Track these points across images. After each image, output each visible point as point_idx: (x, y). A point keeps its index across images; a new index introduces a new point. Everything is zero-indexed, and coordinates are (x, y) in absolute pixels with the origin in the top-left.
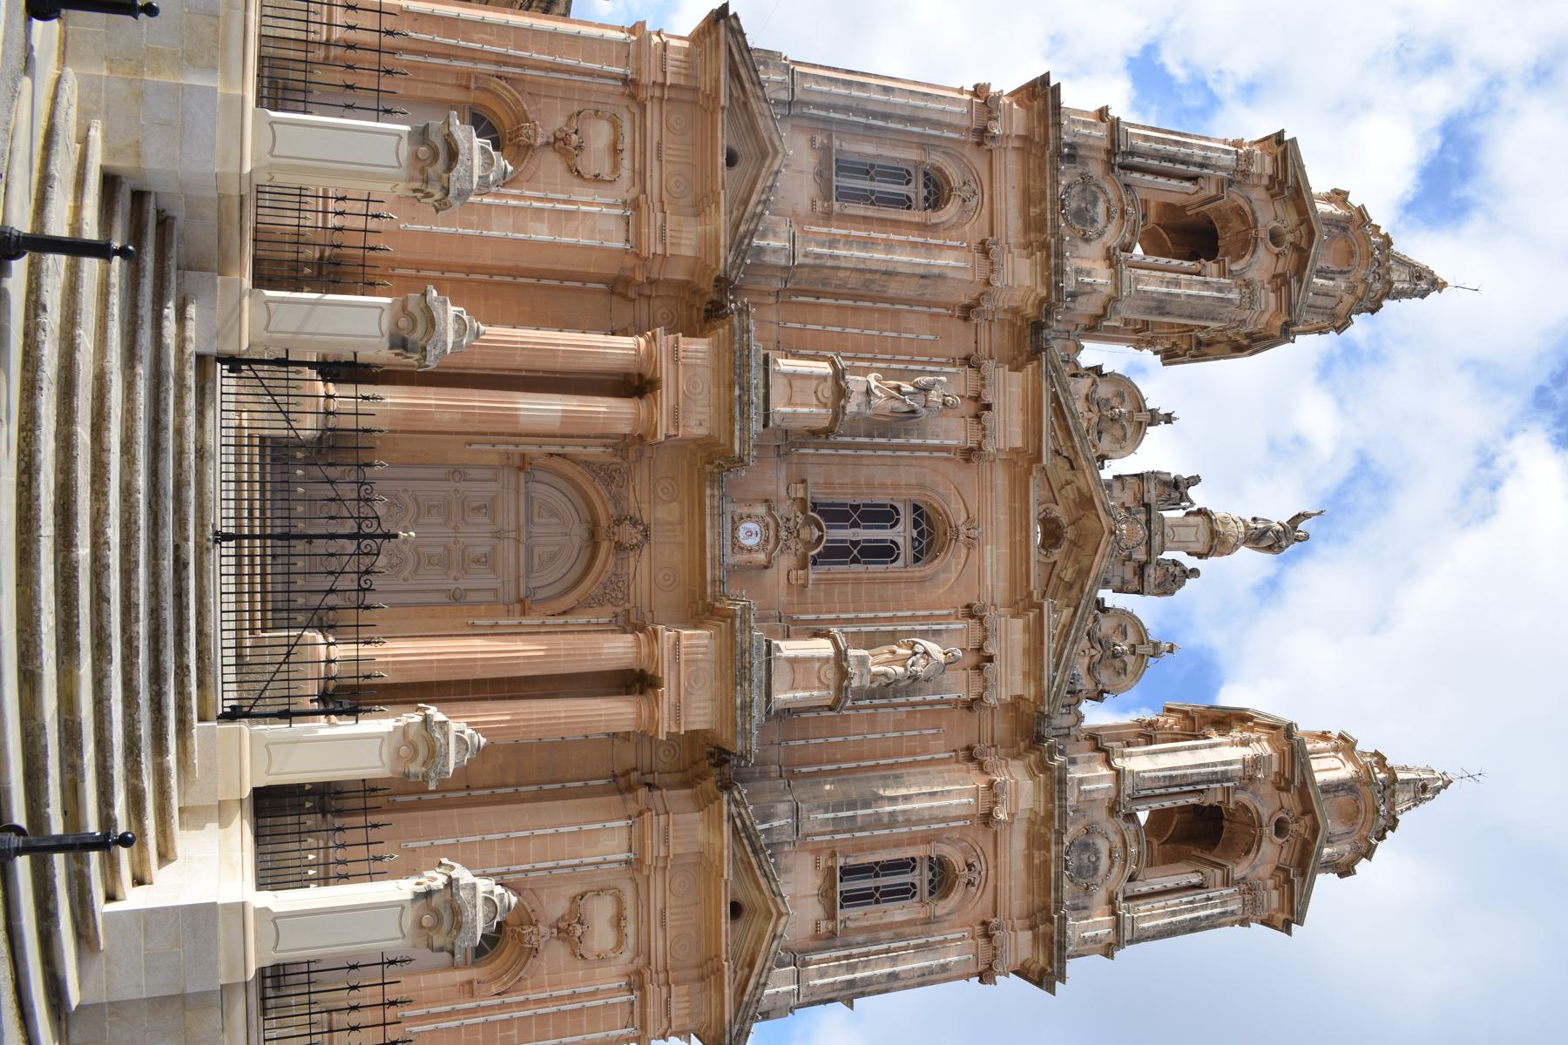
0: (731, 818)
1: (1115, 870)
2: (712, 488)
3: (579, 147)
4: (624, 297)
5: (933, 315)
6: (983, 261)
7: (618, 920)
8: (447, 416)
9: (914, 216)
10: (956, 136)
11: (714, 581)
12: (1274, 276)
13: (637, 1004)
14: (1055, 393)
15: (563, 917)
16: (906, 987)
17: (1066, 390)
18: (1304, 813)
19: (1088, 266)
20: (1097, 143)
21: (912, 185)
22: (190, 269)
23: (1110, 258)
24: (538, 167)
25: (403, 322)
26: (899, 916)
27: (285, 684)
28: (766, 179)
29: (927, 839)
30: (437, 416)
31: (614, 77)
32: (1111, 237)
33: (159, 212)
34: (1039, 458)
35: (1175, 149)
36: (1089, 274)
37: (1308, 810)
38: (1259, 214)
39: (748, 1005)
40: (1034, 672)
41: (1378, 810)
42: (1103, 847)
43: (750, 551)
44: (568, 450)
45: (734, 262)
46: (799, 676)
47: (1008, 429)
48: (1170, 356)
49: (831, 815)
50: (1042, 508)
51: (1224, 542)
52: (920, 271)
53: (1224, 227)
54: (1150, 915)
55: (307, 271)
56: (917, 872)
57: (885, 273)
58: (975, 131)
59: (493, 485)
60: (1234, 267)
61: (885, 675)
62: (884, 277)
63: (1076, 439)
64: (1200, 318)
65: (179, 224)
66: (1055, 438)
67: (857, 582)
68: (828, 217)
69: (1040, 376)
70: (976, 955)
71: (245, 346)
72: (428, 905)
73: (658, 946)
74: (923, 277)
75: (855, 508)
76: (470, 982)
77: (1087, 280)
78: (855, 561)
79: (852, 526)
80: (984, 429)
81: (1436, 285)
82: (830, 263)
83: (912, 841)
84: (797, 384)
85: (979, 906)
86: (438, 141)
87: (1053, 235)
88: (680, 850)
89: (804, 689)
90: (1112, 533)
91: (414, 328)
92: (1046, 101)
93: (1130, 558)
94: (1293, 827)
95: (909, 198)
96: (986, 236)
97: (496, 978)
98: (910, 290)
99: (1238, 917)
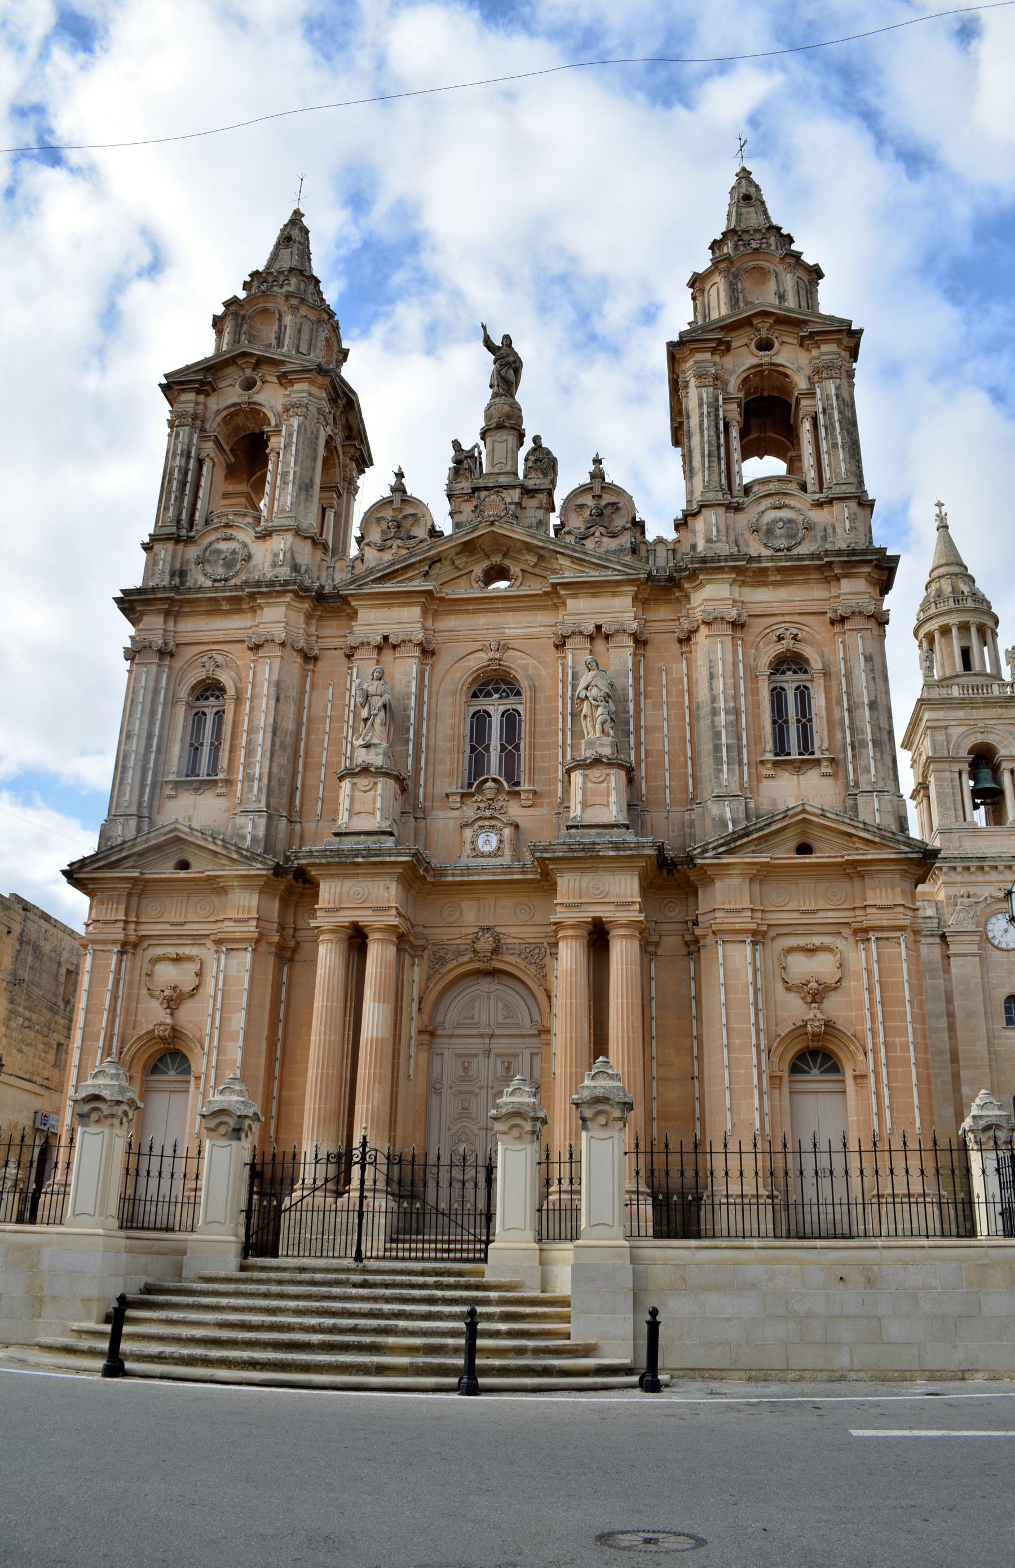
0: (717, 856)
1: (792, 502)
2: (446, 875)
3: (175, 988)
4: (295, 950)
5: (312, 688)
6: (266, 649)
7: (811, 951)
8: (376, 1095)
9: (230, 709)
10: (165, 676)
11: (523, 873)
12: (281, 384)
13: (879, 935)
14: (374, 581)
15: (803, 998)
16: (887, 692)
17: (371, 571)
18: (751, 325)
19: (268, 557)
20: (170, 553)
21: (206, 710)
22: (181, 1275)
23: (265, 536)
24: (190, 1022)
25: (223, 1130)
26: (822, 702)
27: (466, 1217)
28: (195, 837)
29: (753, 677)
30: (376, 1103)
31: (120, 962)
32: (245, 535)
33: (142, 1293)
34: (429, 593)
35: (175, 483)
36: (276, 555)
37: (746, 322)
38: (229, 402)
39: (883, 837)
40: (610, 587)
41: (757, 249)
42: (772, 515)
43: (501, 841)
44: (415, 995)
45: (261, 862)
46: (598, 800)
47: (405, 620)
48: (363, 461)
49: (725, 767)
50: (475, 585)
51: (508, 417)
52: (273, 702)
53: (243, 429)
54: (836, 467)
55: (265, 1203)
56: (785, 685)
57: (274, 733)
58: (161, 659)
59: (446, 1056)
60: (273, 423)
61: (603, 724)
62: (278, 733)
63: (413, 560)
64: (315, 450)
65: (150, 1280)
66: (410, 579)
67: (533, 746)
68: (229, 782)
69: (360, 595)
70: (859, 630)
71: (233, 1239)
72: (591, 1120)
73: (832, 916)
74: (278, 700)
75: (473, 749)
76: (855, 1077)
77: (281, 557)
78: (517, 747)
79: (488, 752)
80: (404, 641)
81: (297, 218)
82: (265, 780)
83: (754, 692)
84: (357, 808)
85: (817, 628)
86: (87, 1108)
87: (243, 590)
88: (747, 899)
89: (609, 795)
90: (492, 523)
91: (225, 1123)
92: (136, 600)
93: (519, 504)
94: (764, 333)
95: (217, 713)
96: (245, 646)
97: (853, 1055)
98: (290, 712)
99: (845, 381)
